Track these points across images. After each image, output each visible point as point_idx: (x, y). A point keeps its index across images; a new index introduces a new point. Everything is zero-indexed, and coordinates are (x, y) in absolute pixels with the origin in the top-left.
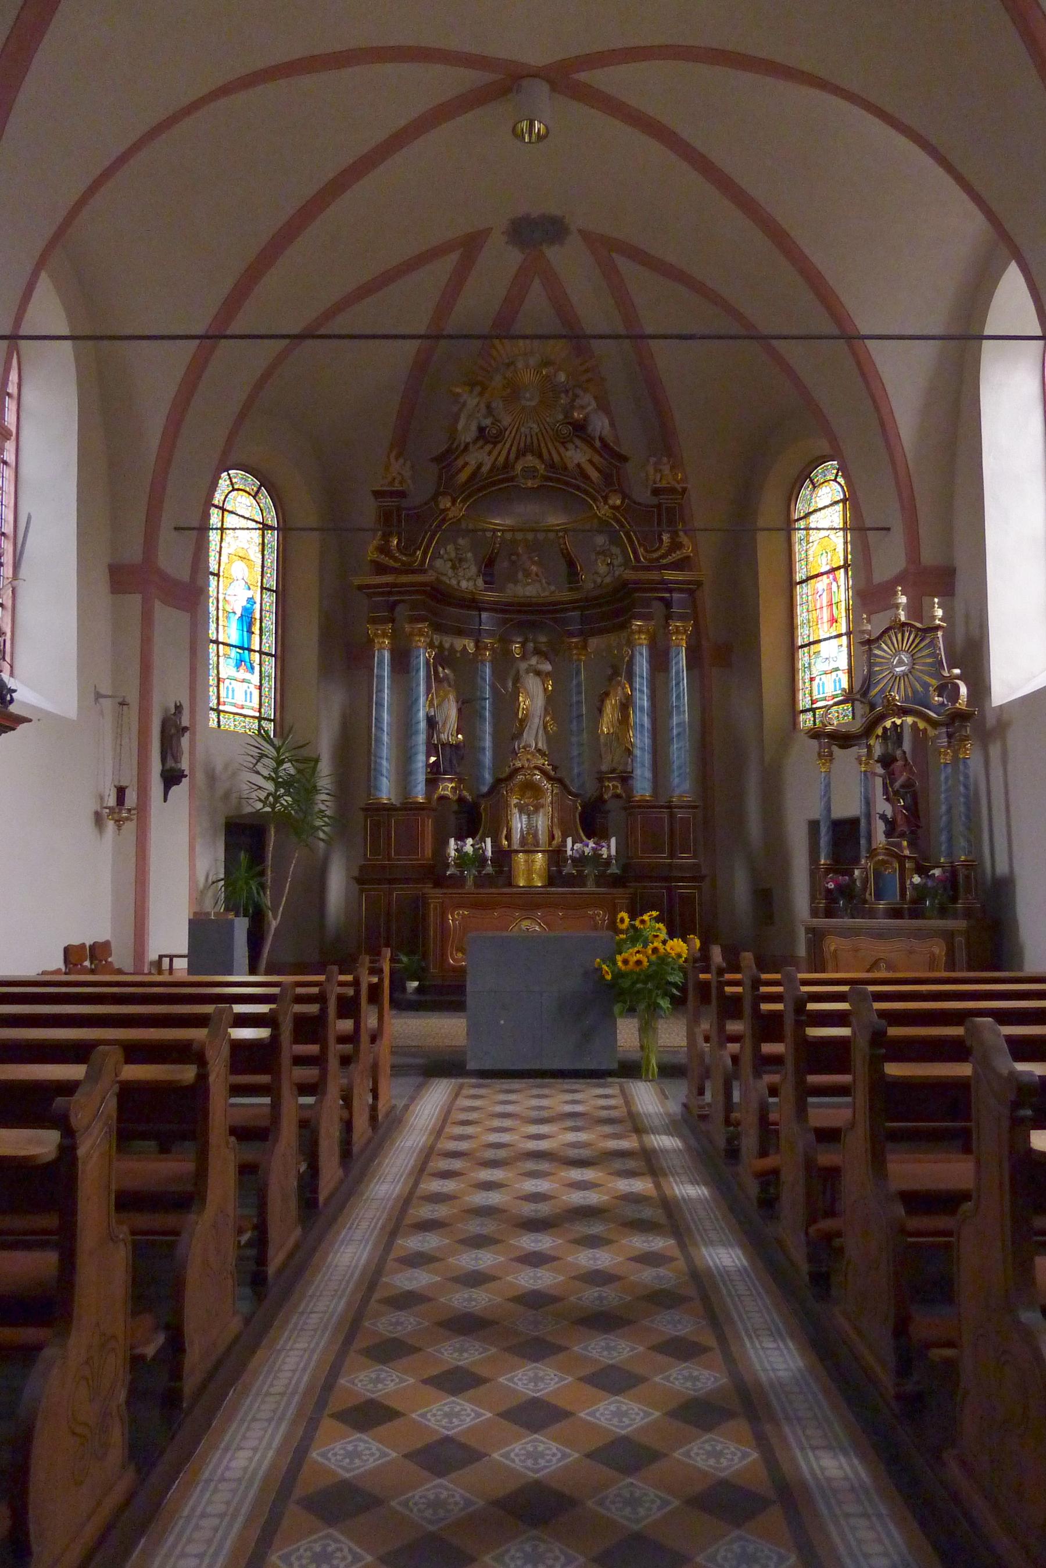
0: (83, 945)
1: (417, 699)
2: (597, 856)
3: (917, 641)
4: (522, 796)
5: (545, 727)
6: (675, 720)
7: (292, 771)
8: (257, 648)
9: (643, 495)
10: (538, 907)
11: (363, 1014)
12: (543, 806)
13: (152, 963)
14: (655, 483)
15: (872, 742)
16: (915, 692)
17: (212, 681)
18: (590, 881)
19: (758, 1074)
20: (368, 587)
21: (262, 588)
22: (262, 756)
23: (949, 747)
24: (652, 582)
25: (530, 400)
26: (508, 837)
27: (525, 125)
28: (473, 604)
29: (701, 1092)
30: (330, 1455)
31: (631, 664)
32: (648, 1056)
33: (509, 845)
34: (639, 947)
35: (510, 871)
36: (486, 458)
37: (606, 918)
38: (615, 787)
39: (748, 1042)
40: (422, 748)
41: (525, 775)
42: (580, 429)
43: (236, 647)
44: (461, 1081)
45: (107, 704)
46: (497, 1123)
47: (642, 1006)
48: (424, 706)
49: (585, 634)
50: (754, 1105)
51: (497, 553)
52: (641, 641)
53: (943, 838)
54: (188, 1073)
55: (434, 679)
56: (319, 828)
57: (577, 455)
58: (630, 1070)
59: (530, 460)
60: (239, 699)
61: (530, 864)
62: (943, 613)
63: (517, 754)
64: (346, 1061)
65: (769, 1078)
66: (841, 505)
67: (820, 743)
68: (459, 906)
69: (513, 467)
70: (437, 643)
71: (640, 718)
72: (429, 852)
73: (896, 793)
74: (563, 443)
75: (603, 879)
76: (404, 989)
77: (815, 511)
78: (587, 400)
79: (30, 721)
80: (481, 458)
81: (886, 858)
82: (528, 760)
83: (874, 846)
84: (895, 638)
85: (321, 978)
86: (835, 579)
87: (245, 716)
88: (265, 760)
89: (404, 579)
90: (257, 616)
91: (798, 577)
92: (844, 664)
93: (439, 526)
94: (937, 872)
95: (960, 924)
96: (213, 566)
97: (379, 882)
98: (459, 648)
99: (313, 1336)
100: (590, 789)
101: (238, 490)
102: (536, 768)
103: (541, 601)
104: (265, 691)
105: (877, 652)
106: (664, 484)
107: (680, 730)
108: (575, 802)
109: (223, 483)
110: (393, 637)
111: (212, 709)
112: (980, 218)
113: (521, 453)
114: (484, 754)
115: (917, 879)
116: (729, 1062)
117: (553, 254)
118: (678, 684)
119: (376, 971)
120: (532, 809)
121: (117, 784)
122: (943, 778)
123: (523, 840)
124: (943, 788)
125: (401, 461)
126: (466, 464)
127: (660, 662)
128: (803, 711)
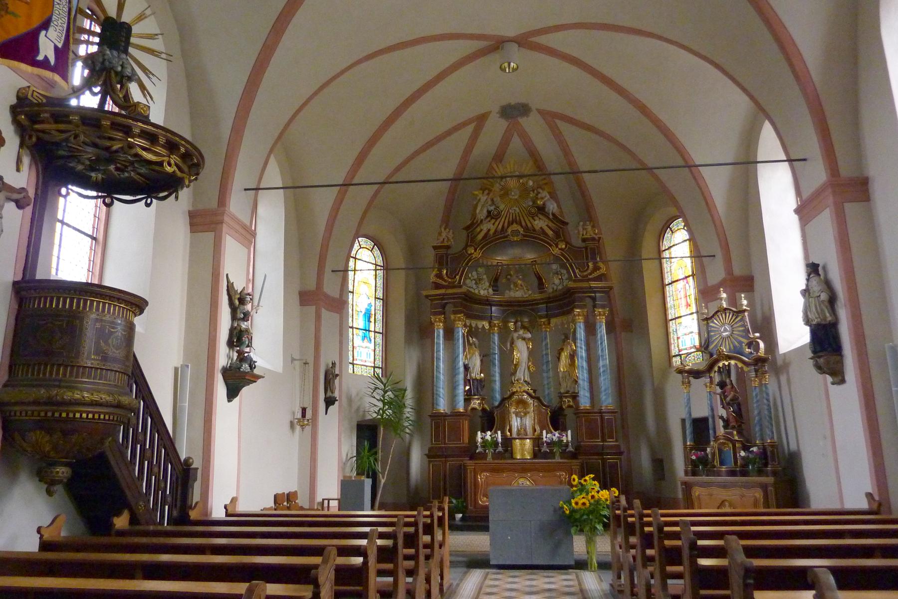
0: (284, 493)
1: (458, 356)
2: (560, 441)
3: (733, 318)
4: (517, 407)
6: (601, 363)
7: (392, 396)
8: (373, 330)
9: (577, 242)
10: (530, 470)
11: (435, 532)
12: (529, 413)
13: (318, 503)
15: (712, 375)
16: (735, 347)
17: (350, 348)
18: (557, 455)
19: (645, 566)
20: (430, 296)
21: (376, 298)
22: (376, 388)
23: (756, 377)
24: (586, 288)
25: (515, 195)
26: (510, 431)
27: (506, 64)
28: (488, 302)
29: (619, 577)
31: (575, 332)
32: (591, 557)
33: (511, 435)
34: (584, 495)
38: (569, 401)
39: (639, 547)
40: (462, 382)
42: (542, 210)
43: (362, 329)
44: (487, 570)
45: (297, 363)
47: (587, 528)
48: (462, 359)
49: (549, 317)
50: (643, 582)
52: (579, 320)
53: (757, 429)
54: (359, 560)
55: (467, 344)
56: (407, 427)
57: (540, 223)
58: (581, 565)
59: (515, 227)
60: (364, 357)
61: (523, 445)
62: (748, 302)
63: (513, 384)
64: (428, 558)
65: (651, 569)
66: (688, 242)
67: (683, 376)
70: (468, 324)
71: (581, 362)
72: (466, 440)
73: (728, 404)
74: (533, 218)
75: (564, 454)
76: (454, 518)
77: (674, 245)
78: (545, 194)
79: (263, 377)
80: (489, 226)
81: (724, 441)
82: (519, 387)
83: (717, 435)
84: (721, 316)
85: (415, 513)
86: (687, 283)
87: (367, 366)
88: (377, 391)
89: (450, 291)
90: (373, 313)
91: (667, 281)
92: (696, 330)
93: (467, 264)
94: (755, 449)
95: (770, 480)
96: (351, 288)
97: (439, 456)
98: (480, 326)
100: (555, 403)
101: (363, 248)
102: (524, 391)
103: (523, 299)
104: (377, 352)
105: (712, 324)
106: (588, 236)
107: (605, 369)
108: (546, 410)
109: (356, 246)
110: (445, 322)
111: (350, 363)
112: (746, 98)
113: (510, 223)
114: (496, 384)
115: (743, 454)
116: (632, 559)
117: (523, 121)
118: (601, 343)
119: (441, 509)
121: (302, 406)
122: (754, 394)
123: (519, 433)
124: (755, 400)
125: (448, 230)
126: (482, 230)
127: (591, 329)
128: (674, 356)
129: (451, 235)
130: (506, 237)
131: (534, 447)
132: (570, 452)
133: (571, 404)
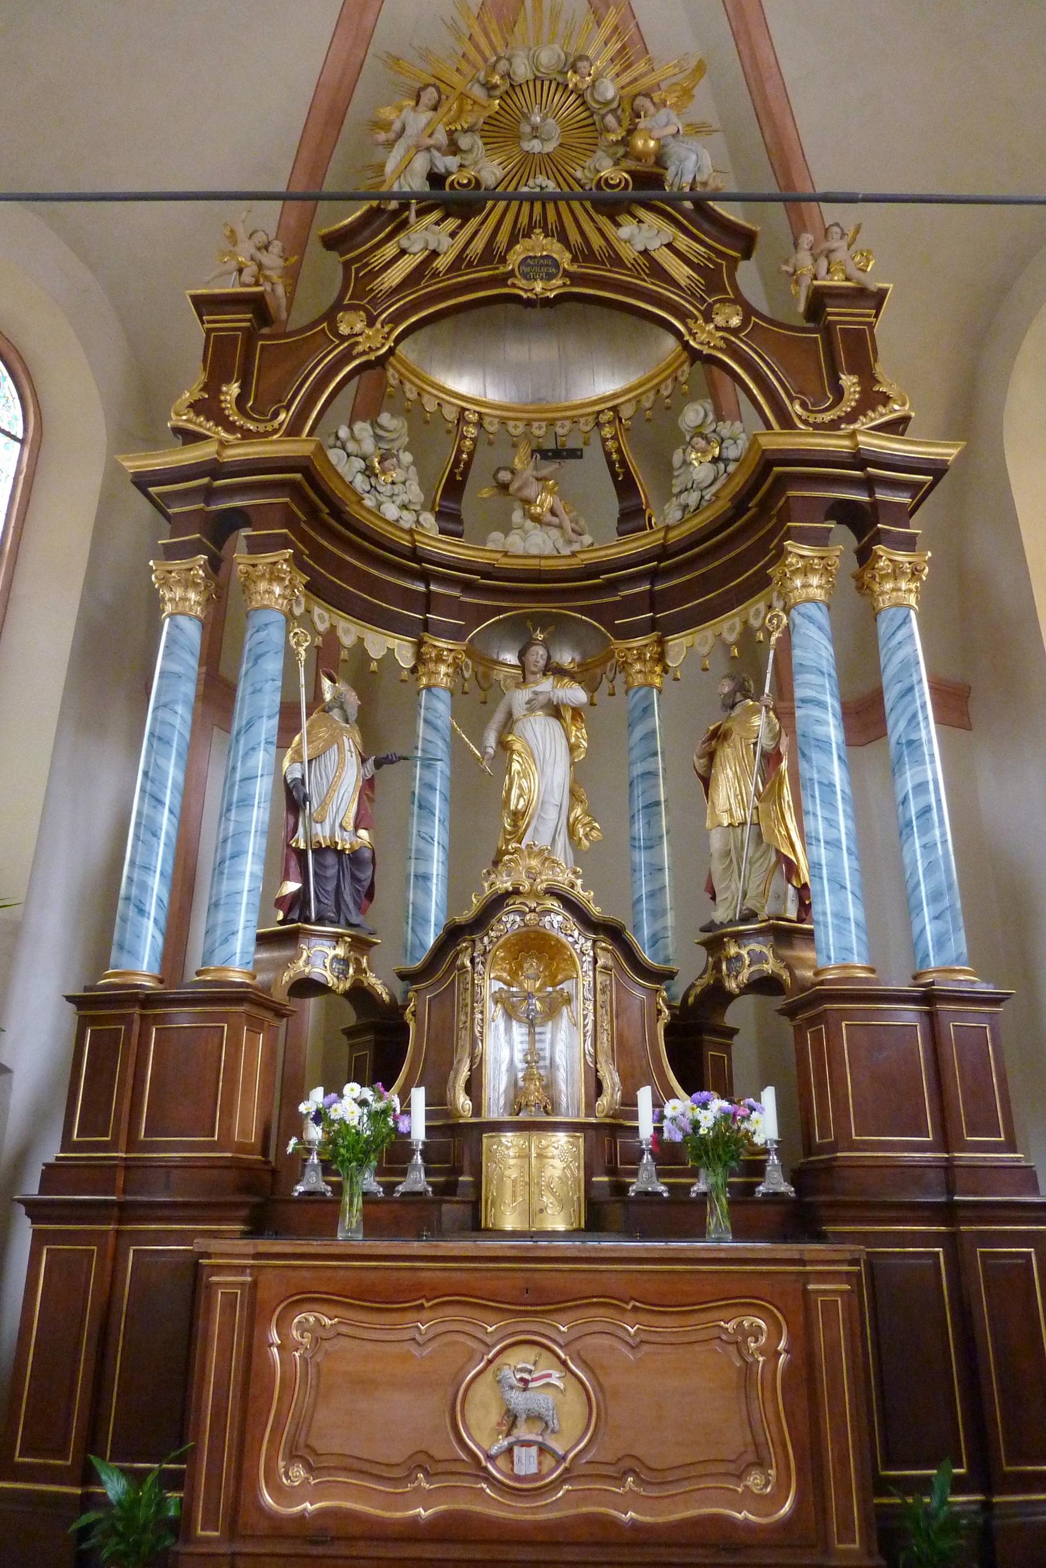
5: (571, 832)
14: (815, 278)
18: (718, 1218)
26: (474, 1087)
33: (477, 1110)
35: (477, 1185)
36: (446, 241)
37: (782, 1345)
38: (760, 958)
41: (522, 914)
51: (468, 464)
68: (304, 1299)
69: (503, 260)
102: (552, 892)
120: (538, 1005)
123: (517, 1101)
130: (502, 280)
131: (589, 1172)
132: (775, 1198)
133: (769, 967)
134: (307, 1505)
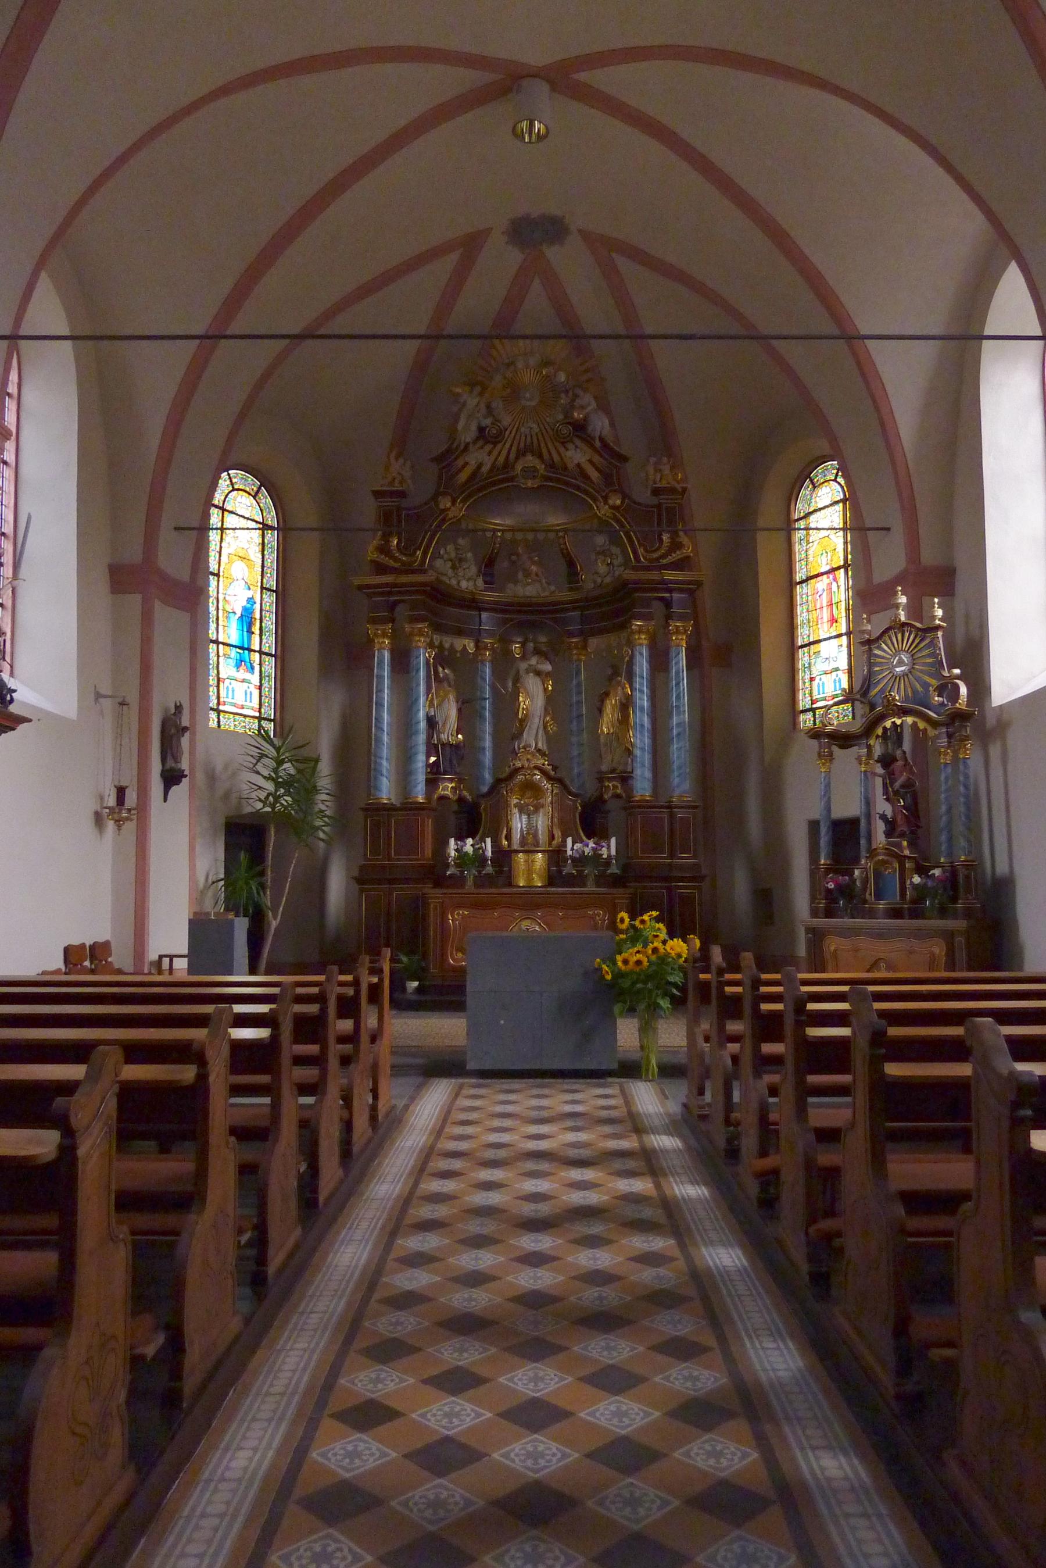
0: (83, 945)
1: (417, 699)
2: (597, 856)
3: (917, 641)
4: (522, 796)
5: (545, 727)
6: (675, 720)
7: (292, 771)
8: (257, 648)
9: (643, 495)
10: (538, 907)
11: (363, 1014)
12: (543, 806)
13: (152, 963)
14: (655, 483)
15: (872, 742)
16: (915, 692)
17: (212, 681)
18: (590, 881)
19: (758, 1074)
20: (368, 587)
21: (262, 588)
22: (262, 756)
23: (949, 747)
24: (652, 582)
25: (530, 400)
26: (508, 837)
27: (525, 125)
28: (473, 604)
29: (701, 1092)
30: (330, 1455)
31: (631, 664)
32: (648, 1056)
33: (509, 845)
34: (639, 947)
35: (510, 871)
36: (486, 458)
37: (606, 918)
38: (615, 787)
39: (748, 1042)
40: (422, 748)
41: (525, 775)
42: (580, 429)
43: (236, 647)
44: (461, 1081)
45: (107, 704)
46: (497, 1123)
47: (642, 1006)
48: (424, 706)
49: (585, 634)
50: (754, 1105)
51: (497, 553)
52: (641, 641)
53: (943, 838)
54: (188, 1073)
55: (434, 679)
56: (319, 828)
57: (577, 455)
58: (630, 1070)
59: (530, 460)
60: (239, 699)
61: (530, 864)
62: (943, 613)
63: (517, 754)
64: (346, 1061)
65: (769, 1078)
66: (841, 505)
67: (820, 743)
68: (459, 906)
69: (513, 467)
70: (437, 643)
71: (640, 718)
72: (429, 852)
73: (896, 793)
74: (563, 443)
75: (603, 879)
76: (404, 989)
77: (815, 511)
78: (587, 400)
79: (30, 721)
80: (481, 458)
81: (886, 858)
82: (528, 760)
83: (874, 846)
84: (895, 638)
85: (321, 978)
86: (835, 579)
87: (245, 716)
88: (265, 760)
89: (404, 579)
90: (257, 616)
91: (798, 577)
92: (844, 664)
93: (439, 526)
94: (937, 872)
95: (960, 924)
96: (213, 566)
97: (379, 882)
98: (459, 648)
99: (313, 1336)
100: (590, 789)
101: (238, 490)
102: (536, 768)
103: (541, 601)
104: (265, 691)
105: (877, 652)
106: (664, 484)
107: (680, 730)
108: (575, 802)
109: (223, 483)
110: (393, 637)
111: (212, 709)
112: (980, 218)
113: (521, 453)
114: (484, 754)
115: (917, 879)
116: (729, 1062)
117: (553, 254)
118: (678, 684)
119: (376, 971)
120: (532, 809)
121: (117, 784)
122: (943, 778)
123: (523, 840)
124: (943, 788)
125: (401, 461)
126: (466, 464)
127: (660, 662)
128: (803, 711)
129: (407, 473)
130: (512, 479)
134: (464, 963)
